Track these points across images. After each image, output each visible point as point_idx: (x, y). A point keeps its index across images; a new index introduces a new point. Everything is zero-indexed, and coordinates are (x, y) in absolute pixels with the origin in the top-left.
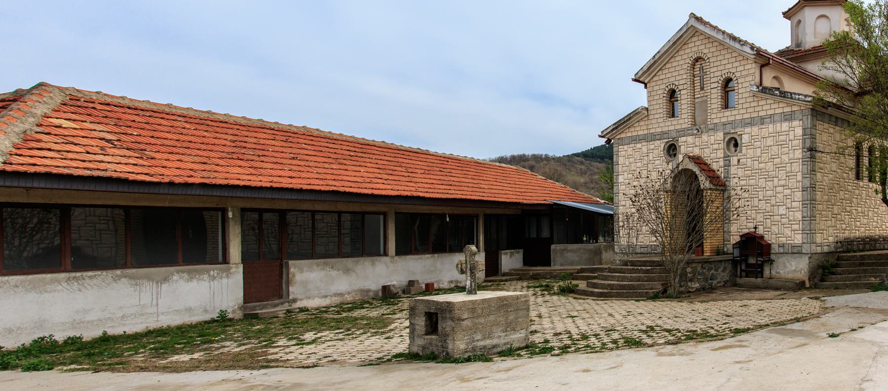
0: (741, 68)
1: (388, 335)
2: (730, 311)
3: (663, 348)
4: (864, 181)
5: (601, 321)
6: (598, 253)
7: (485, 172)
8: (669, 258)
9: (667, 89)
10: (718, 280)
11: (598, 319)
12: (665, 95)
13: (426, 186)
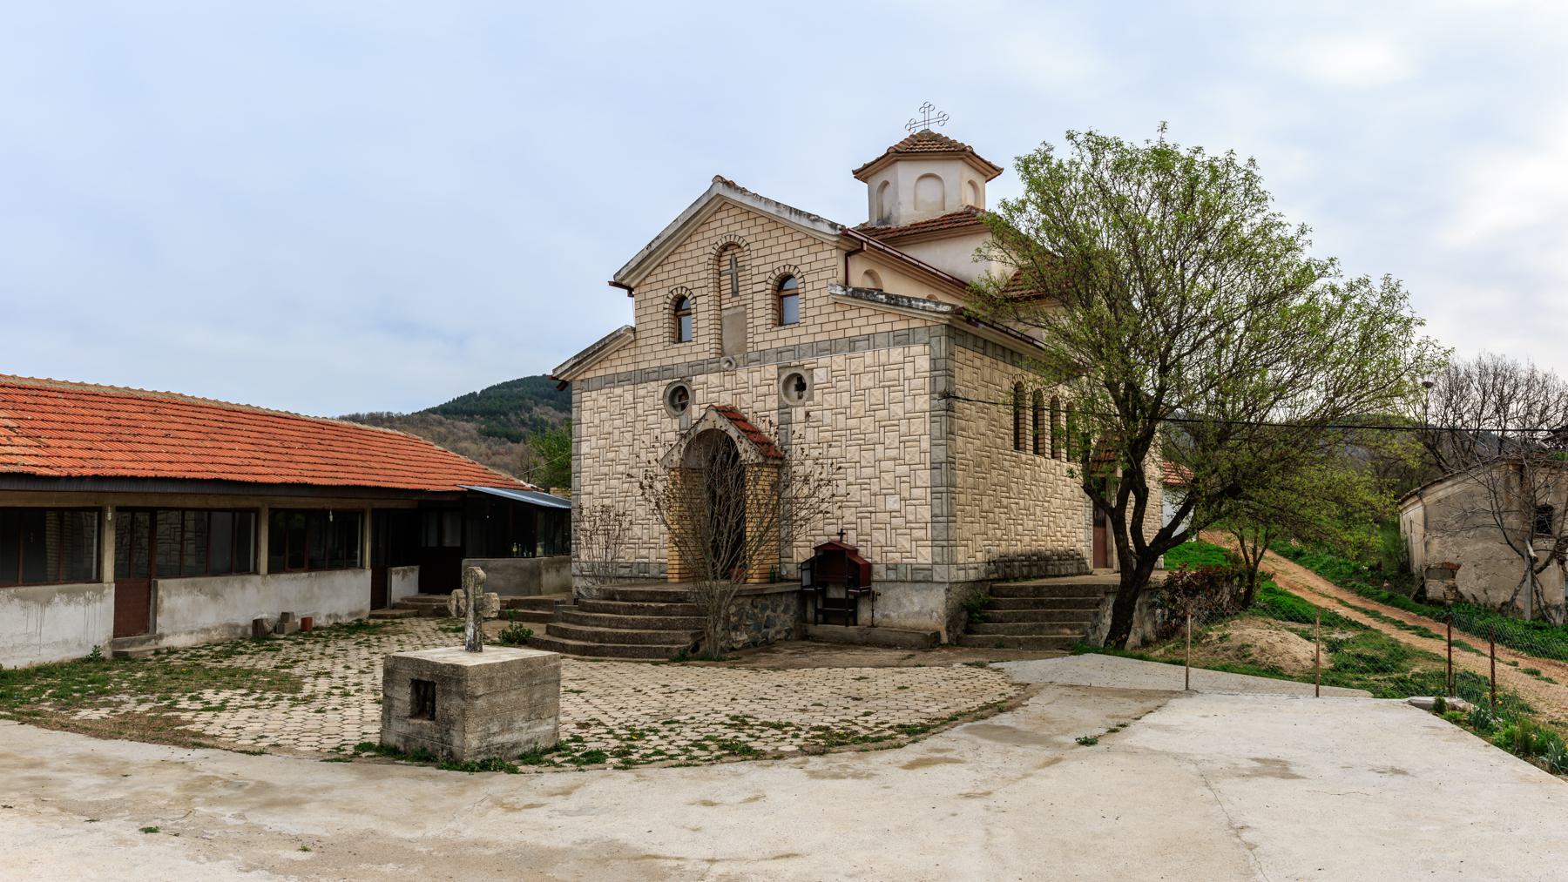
0: (812, 258)
6: (535, 573)
7: (369, 443)
9: (671, 296)
10: (778, 628)
12: (667, 306)
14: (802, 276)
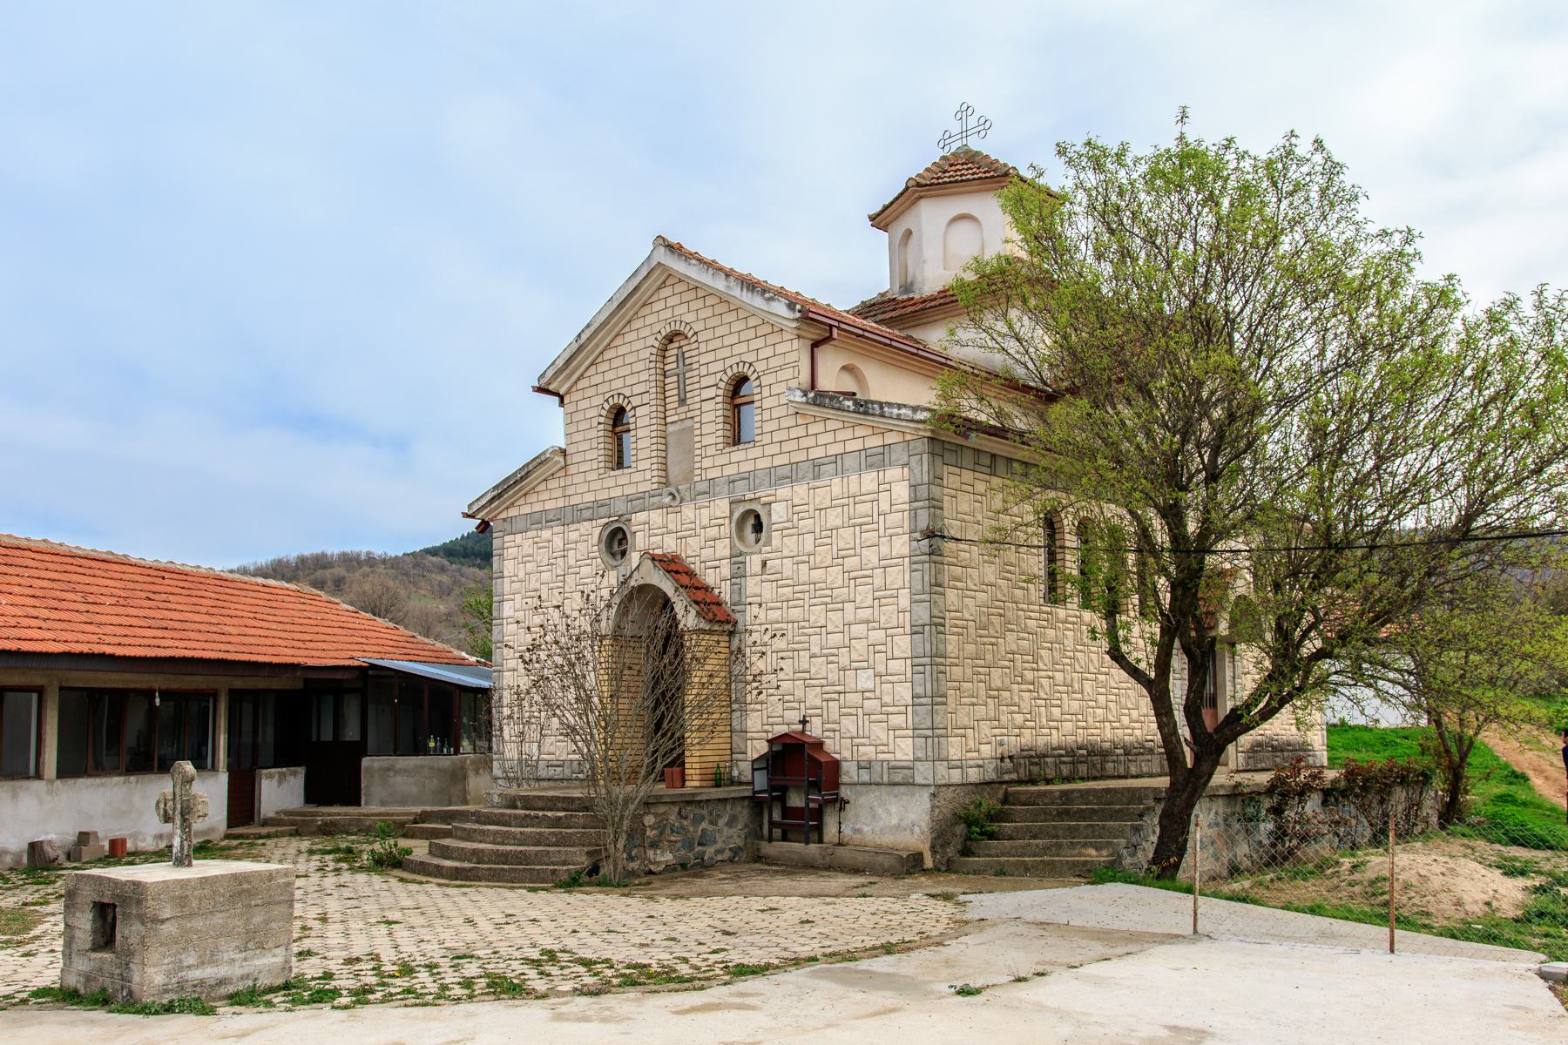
0: (768, 352)
1: (27, 948)
2: (734, 923)
3: (566, 1003)
4: (1069, 606)
5: (447, 935)
6: (458, 777)
8: (603, 791)
9: (607, 406)
10: (719, 845)
11: (441, 929)
13: (119, 631)
14: (758, 378)
